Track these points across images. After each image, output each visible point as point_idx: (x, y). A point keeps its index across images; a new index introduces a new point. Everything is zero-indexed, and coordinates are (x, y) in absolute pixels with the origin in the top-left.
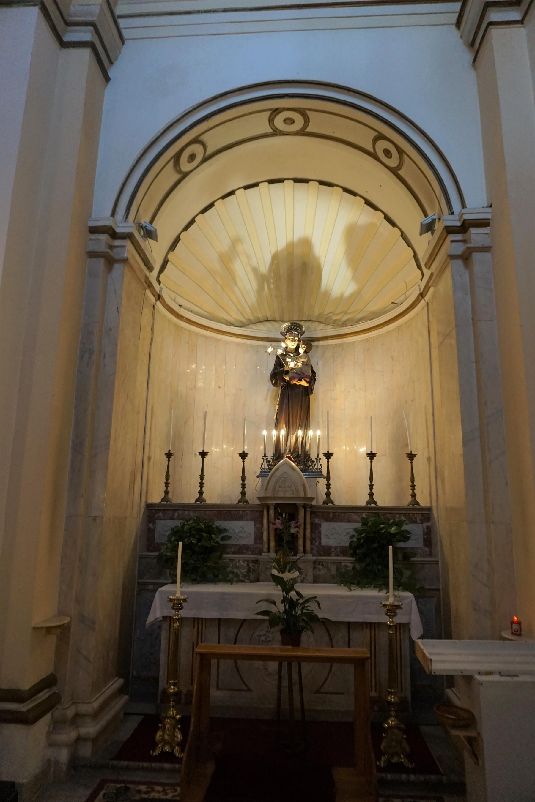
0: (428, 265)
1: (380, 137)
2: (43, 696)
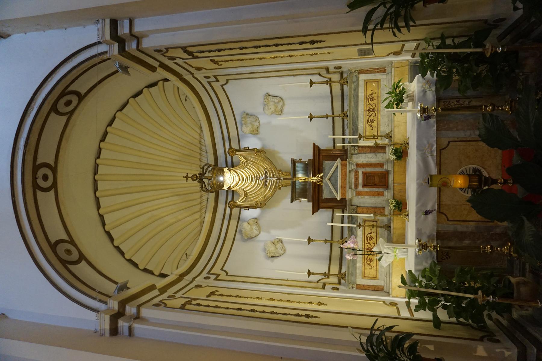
0: (153, 69)
1: (54, 109)
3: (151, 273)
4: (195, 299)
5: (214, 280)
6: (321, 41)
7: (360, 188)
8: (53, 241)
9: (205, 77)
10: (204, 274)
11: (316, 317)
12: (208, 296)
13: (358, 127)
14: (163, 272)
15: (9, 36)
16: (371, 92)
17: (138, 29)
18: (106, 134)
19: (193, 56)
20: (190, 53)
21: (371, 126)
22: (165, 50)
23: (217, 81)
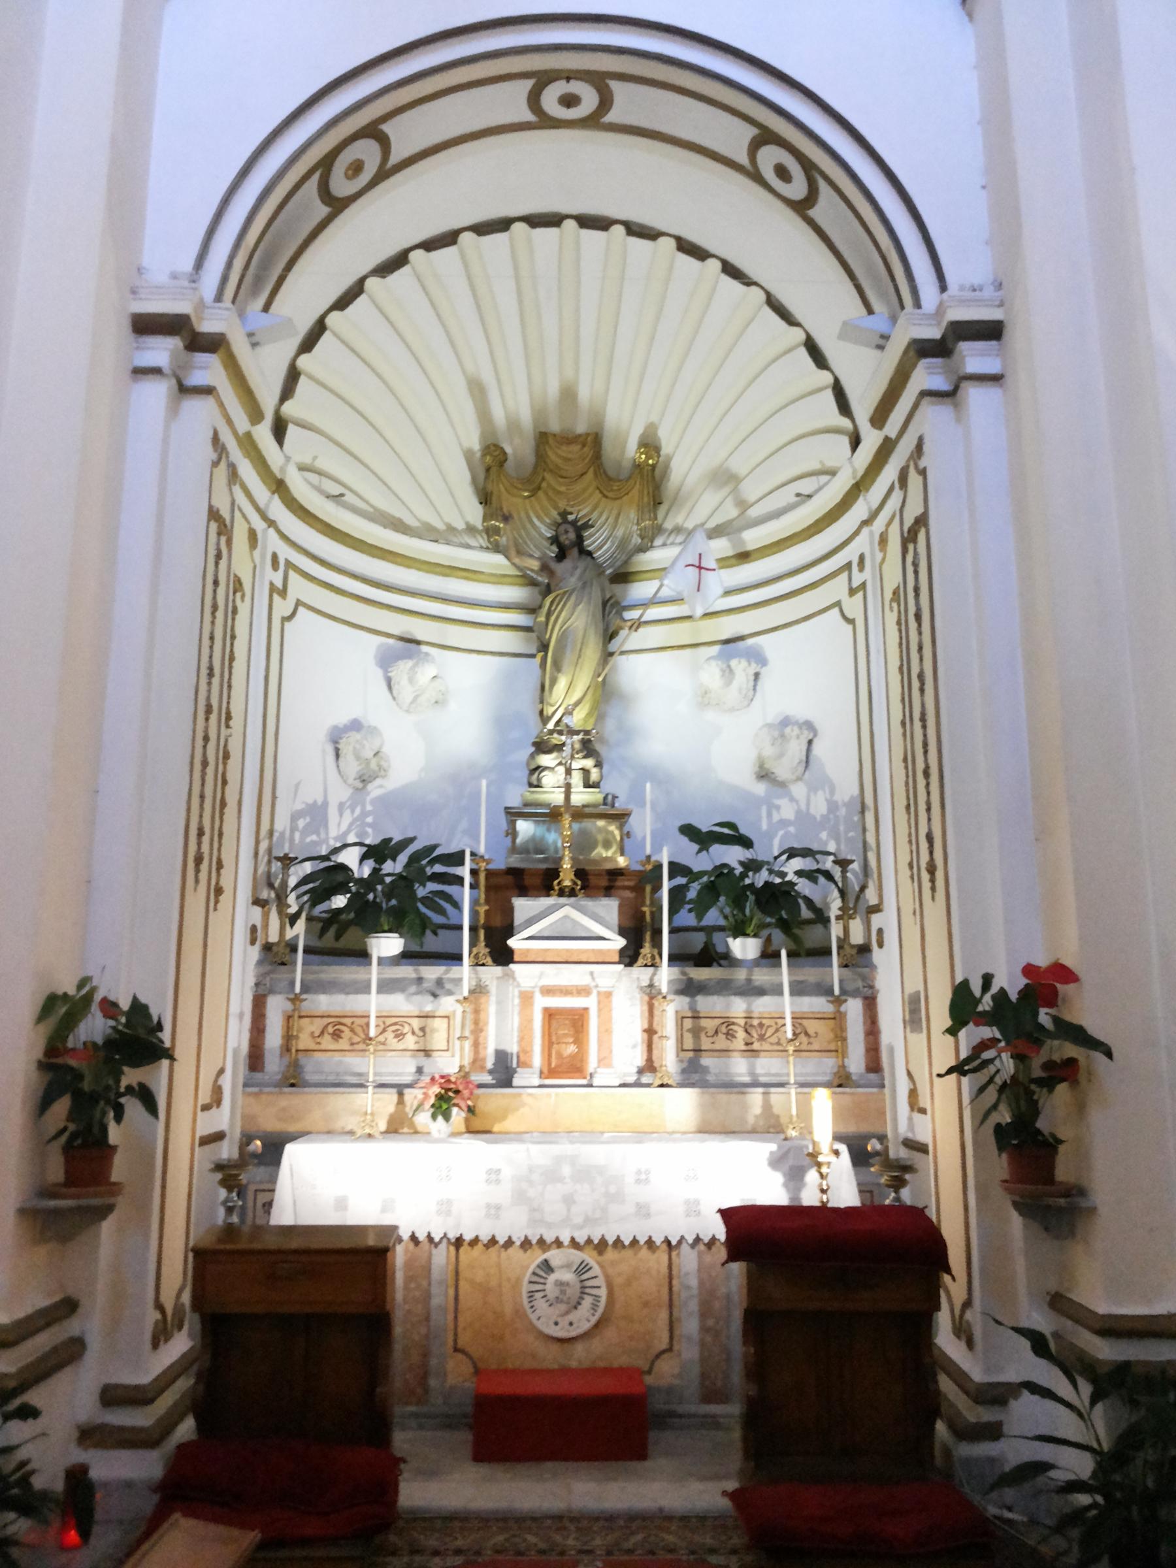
0: (879, 418)
1: (766, 137)
2: (42, 1342)
5: (271, 584)
6: (933, 889)
7: (542, 1002)
8: (386, 128)
9: (862, 558)
11: (197, 881)
13: (713, 994)
14: (292, 431)
15: (970, 15)
16: (811, 1031)
17: (974, 395)
21: (716, 1032)
23: (852, 592)
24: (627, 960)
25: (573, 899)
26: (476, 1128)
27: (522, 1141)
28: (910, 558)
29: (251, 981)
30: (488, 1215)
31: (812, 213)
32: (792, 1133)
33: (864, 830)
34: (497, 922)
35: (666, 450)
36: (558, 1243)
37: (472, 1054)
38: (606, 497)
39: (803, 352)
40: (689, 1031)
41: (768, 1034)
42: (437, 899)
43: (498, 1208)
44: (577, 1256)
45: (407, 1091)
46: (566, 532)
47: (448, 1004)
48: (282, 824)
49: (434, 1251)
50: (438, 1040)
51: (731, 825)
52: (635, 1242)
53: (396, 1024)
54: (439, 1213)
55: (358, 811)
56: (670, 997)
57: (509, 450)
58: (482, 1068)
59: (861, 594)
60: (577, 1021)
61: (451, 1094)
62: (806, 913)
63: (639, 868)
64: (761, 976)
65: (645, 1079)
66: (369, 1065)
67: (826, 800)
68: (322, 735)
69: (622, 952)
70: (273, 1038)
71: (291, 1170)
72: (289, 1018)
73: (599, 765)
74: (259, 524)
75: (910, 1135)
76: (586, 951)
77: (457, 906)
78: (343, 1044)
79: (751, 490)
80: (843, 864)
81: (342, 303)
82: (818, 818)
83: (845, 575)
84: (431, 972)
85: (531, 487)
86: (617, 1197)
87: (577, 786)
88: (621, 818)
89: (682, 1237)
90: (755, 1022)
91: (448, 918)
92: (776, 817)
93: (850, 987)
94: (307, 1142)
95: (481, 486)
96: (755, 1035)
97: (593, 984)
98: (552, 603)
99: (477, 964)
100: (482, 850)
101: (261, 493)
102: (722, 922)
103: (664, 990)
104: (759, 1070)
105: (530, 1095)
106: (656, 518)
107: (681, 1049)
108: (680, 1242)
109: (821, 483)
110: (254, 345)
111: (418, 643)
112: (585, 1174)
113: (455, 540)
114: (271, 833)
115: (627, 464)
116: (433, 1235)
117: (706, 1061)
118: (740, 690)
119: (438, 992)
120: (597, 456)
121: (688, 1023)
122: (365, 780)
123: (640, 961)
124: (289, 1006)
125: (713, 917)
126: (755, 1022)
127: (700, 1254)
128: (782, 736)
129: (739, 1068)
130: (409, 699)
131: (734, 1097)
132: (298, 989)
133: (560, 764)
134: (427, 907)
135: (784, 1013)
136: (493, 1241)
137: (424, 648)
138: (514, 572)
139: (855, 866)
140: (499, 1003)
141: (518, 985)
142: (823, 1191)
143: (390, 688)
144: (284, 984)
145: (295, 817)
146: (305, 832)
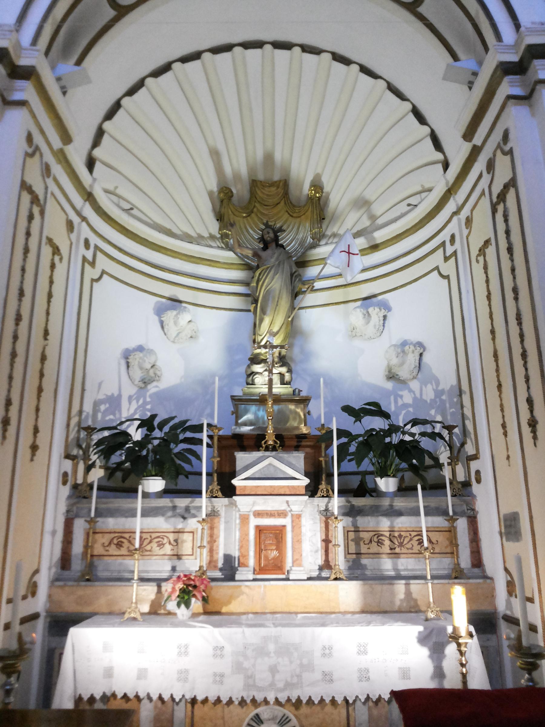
0: (468, 135)
3: (96, 143)
4: (42, 213)
7: (254, 522)
9: (453, 237)
10: (94, 240)
12: (50, 241)
13: (367, 515)
14: (98, 166)
18: (346, 61)
19: (498, 203)
20: (502, 197)
21: (371, 541)
22: (507, 148)
23: (446, 259)
24: (310, 493)
25: (274, 453)
26: (211, 612)
27: (239, 624)
28: (499, 216)
29: (63, 508)
30: (215, 682)
31: (422, 9)
32: (431, 615)
33: (462, 407)
34: (227, 469)
35: (326, 189)
36: (266, 702)
37: (208, 558)
38: (292, 216)
39: (411, 116)
40: (352, 540)
41: (405, 542)
42: (186, 454)
43: (222, 676)
44: (279, 711)
45: (164, 584)
46: (268, 233)
47: (192, 523)
48: (88, 408)
49: (176, 707)
50: (186, 548)
51: (376, 404)
52: (322, 700)
53: (158, 537)
54: (179, 680)
55: (141, 402)
56: (340, 518)
57: (234, 191)
58: (216, 567)
59: (453, 259)
60: (278, 534)
61: (190, 589)
62: (428, 461)
63: (318, 433)
64: (400, 503)
65: (325, 574)
66: (136, 566)
67: (433, 390)
68: (118, 353)
69: (307, 487)
70: (77, 547)
71: (73, 646)
72: (88, 534)
73: (290, 371)
74: (76, 220)
75: (508, 613)
76: (284, 487)
77: (199, 458)
78: (124, 551)
79: (378, 209)
80: (450, 428)
81: (131, 92)
82: (429, 401)
83: (441, 250)
84: (182, 502)
85: (248, 211)
86: (309, 667)
87: (276, 384)
88: (304, 401)
89: (357, 697)
90: (396, 534)
91: (192, 466)
92: (400, 402)
93: (458, 510)
94: (88, 626)
95: (218, 210)
96: (397, 543)
97: (289, 509)
98: (260, 274)
99: (212, 496)
100: (215, 422)
101: (78, 200)
102: (371, 468)
103: (336, 513)
104: (400, 567)
105: (247, 586)
106: (321, 227)
107: (347, 552)
108: (355, 701)
109: (423, 198)
110: (64, 93)
111: (180, 302)
112: (285, 650)
113: (203, 242)
114: (80, 412)
115: (304, 199)
116: (174, 697)
117: (365, 561)
118: (375, 326)
119: (186, 516)
120: (286, 194)
121: (352, 535)
122: (146, 382)
123: (319, 494)
124: (87, 526)
125: (366, 465)
126: (396, 534)
127: (369, 709)
128: (403, 352)
129: (387, 565)
130: (174, 335)
131: (385, 587)
132: (93, 514)
133: (266, 370)
134: (179, 459)
135: (421, 527)
136: (218, 701)
137: (184, 305)
138: (237, 261)
139: (456, 430)
140: (226, 522)
141: (239, 511)
142: (463, 665)
143: (162, 327)
144: (85, 511)
145: (96, 405)
146: (105, 413)
